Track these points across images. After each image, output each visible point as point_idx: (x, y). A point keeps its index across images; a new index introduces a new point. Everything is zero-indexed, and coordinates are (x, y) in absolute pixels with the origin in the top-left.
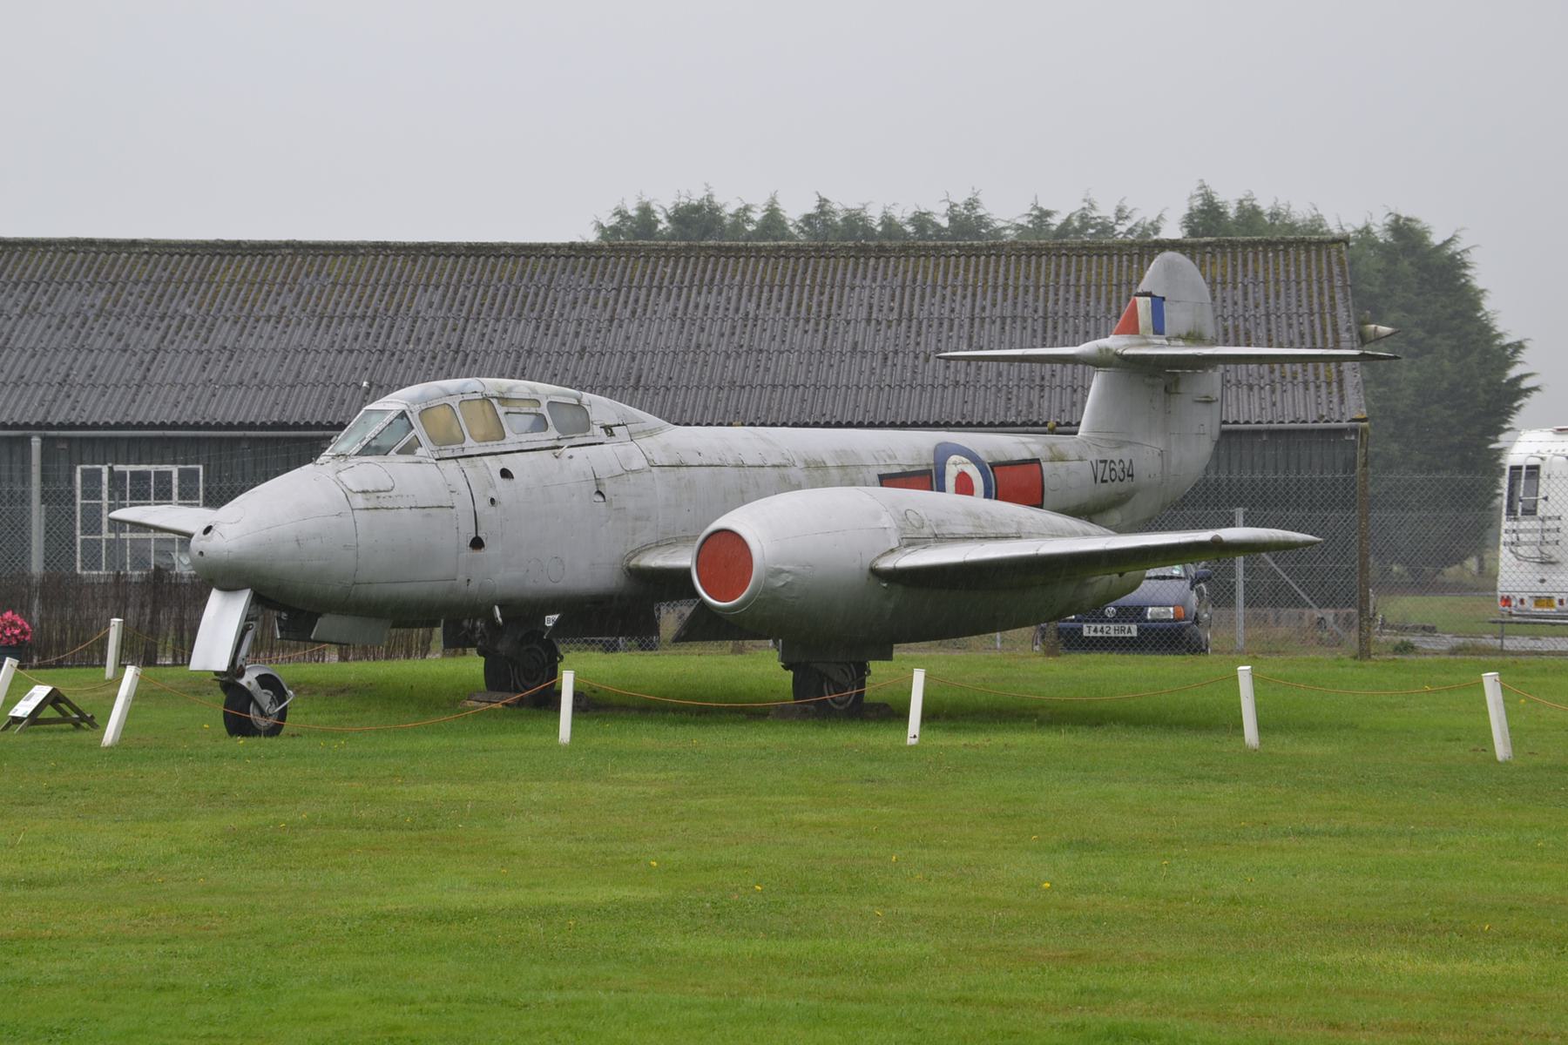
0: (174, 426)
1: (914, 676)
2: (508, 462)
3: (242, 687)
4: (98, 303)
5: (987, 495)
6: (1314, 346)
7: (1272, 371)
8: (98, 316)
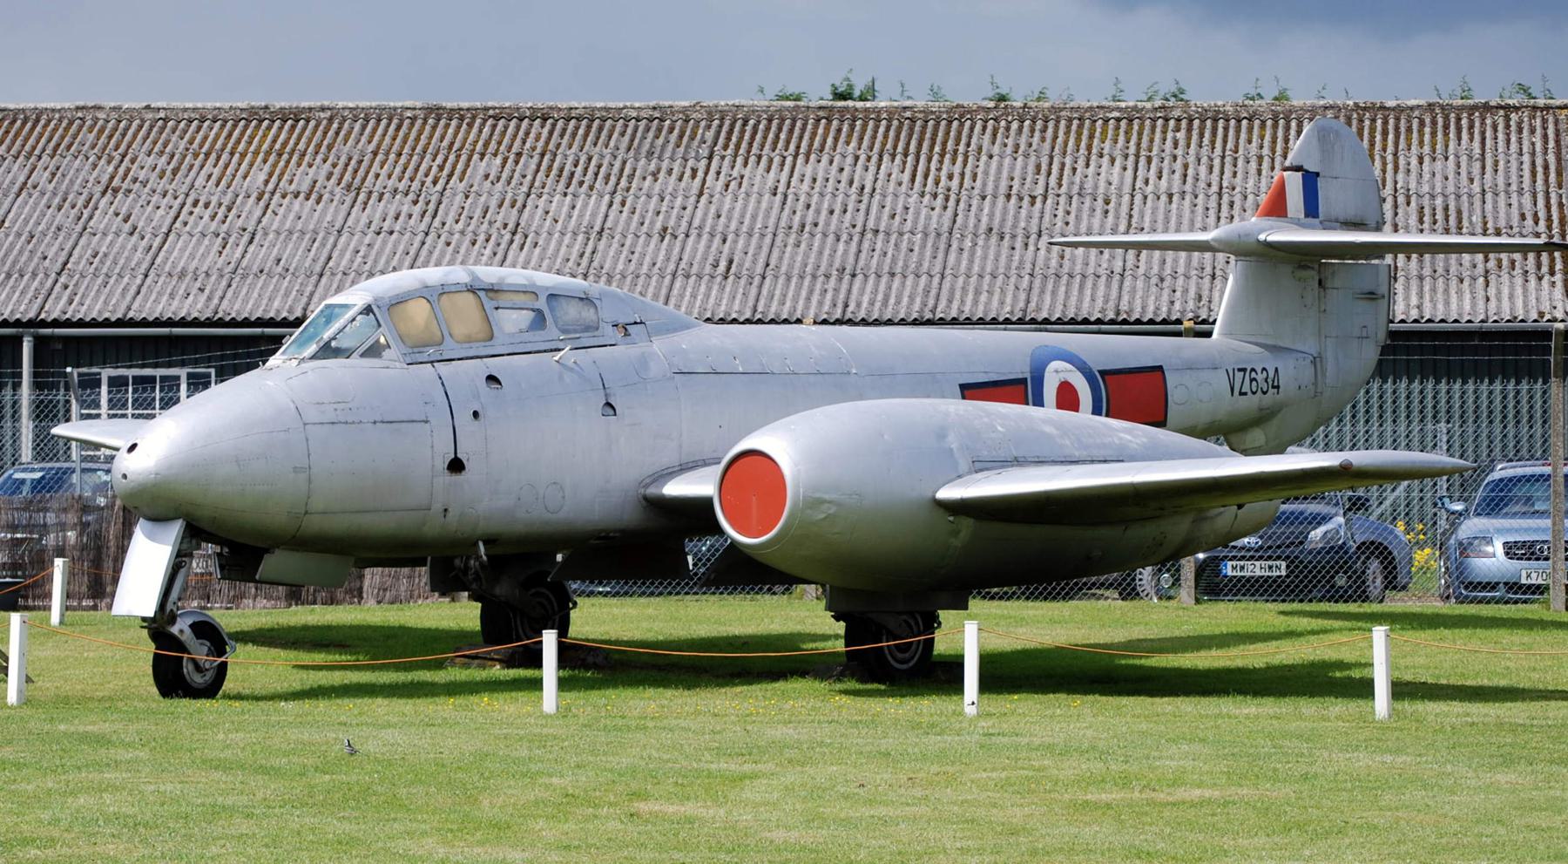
0: (183, 323)
1: (968, 634)
2: (494, 366)
3: (172, 637)
4: (105, 179)
5: (1096, 411)
6: (1447, 231)
7: (1487, 260)
8: (104, 193)
